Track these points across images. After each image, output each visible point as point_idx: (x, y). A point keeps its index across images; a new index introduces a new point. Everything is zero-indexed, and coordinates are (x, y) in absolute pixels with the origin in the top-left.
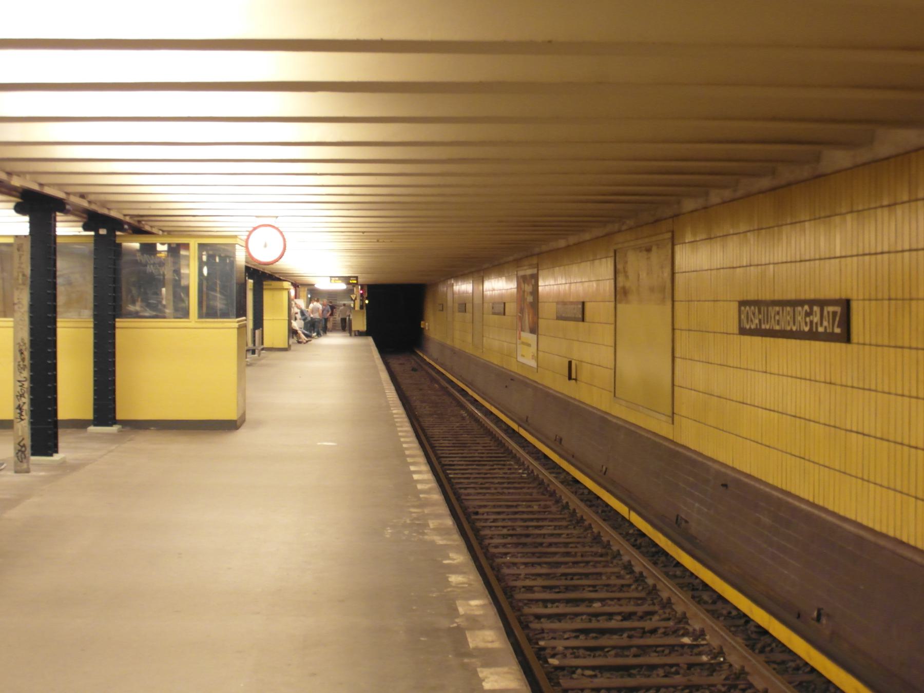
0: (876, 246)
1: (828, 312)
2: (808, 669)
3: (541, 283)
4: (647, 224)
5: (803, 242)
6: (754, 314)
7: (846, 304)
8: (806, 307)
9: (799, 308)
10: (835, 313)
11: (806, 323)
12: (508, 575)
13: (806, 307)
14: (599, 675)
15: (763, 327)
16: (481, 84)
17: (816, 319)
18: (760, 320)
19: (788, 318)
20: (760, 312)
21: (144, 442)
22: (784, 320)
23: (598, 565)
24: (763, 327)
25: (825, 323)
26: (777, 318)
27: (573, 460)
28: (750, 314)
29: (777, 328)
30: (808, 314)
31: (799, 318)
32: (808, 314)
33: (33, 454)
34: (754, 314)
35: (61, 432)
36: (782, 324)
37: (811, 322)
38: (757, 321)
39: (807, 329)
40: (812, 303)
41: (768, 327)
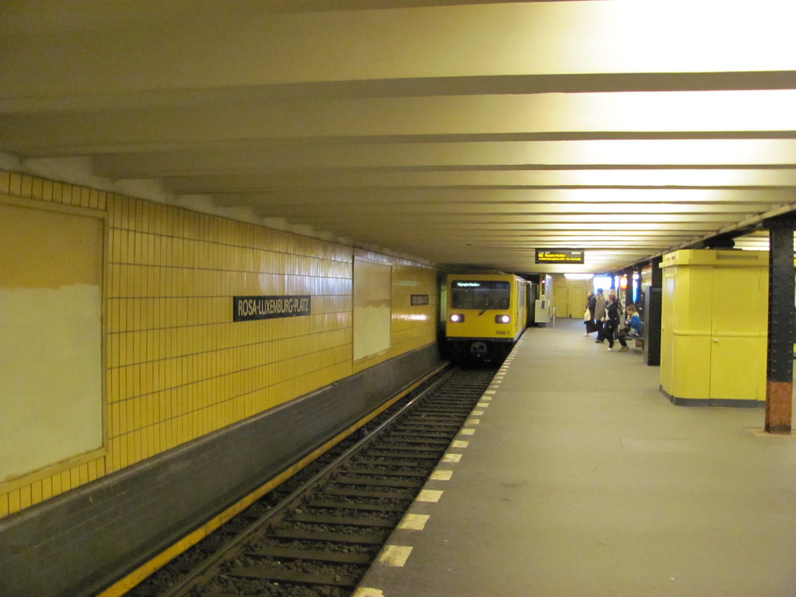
1: (303, 302)
2: (186, 555)
4: (323, 240)
5: (289, 266)
6: (252, 305)
7: (412, 304)
9: (287, 300)
10: (306, 302)
11: (291, 309)
13: (291, 300)
14: (543, 282)
15: (260, 313)
16: (492, 140)
17: (296, 306)
18: (258, 310)
19: (279, 306)
20: (257, 304)
23: (377, 489)
24: (260, 313)
25: (301, 307)
26: (271, 306)
29: (272, 312)
30: (291, 304)
31: (286, 306)
32: (291, 304)
34: (252, 305)
35: (762, 397)
37: (293, 308)
38: (255, 310)
39: (291, 311)
41: (264, 313)
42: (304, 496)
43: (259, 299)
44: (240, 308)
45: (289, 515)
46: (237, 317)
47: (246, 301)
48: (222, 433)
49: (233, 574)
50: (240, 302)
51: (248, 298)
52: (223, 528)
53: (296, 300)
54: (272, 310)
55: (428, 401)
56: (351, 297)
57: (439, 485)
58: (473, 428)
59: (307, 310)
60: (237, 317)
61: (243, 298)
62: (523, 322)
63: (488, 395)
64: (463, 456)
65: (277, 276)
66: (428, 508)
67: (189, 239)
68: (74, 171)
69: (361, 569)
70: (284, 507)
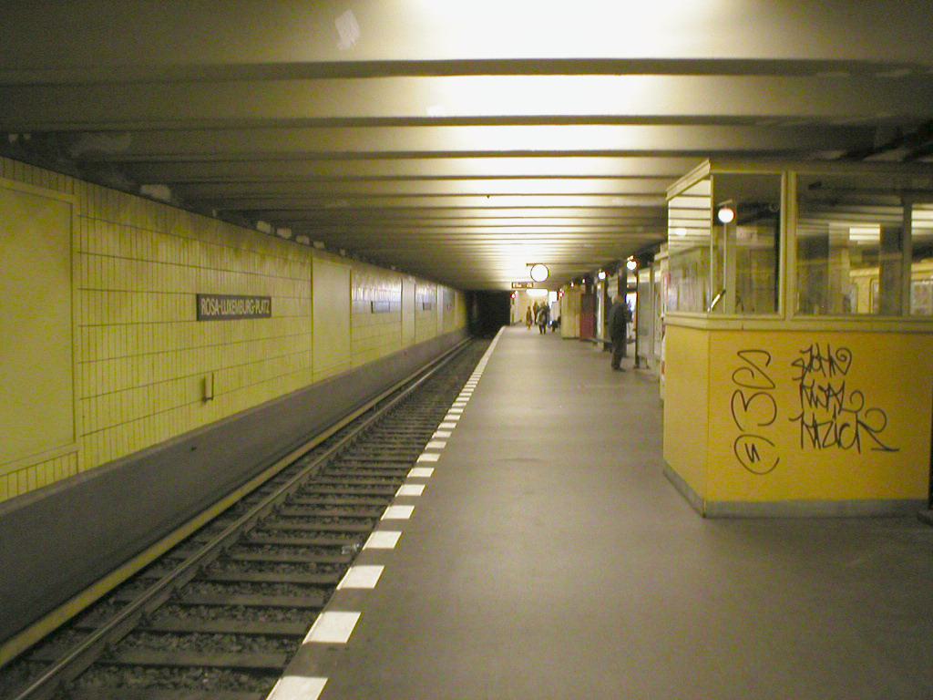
0: (897, 215)
3: (915, 214)
6: (214, 305)
8: (252, 301)
12: (897, 206)
15: (223, 313)
17: (257, 307)
18: (220, 310)
20: (219, 303)
21: (825, 421)
22: (238, 307)
24: (223, 313)
27: (249, 476)
28: (211, 304)
30: (252, 305)
31: (248, 307)
33: (797, 176)
34: (214, 305)
36: (237, 311)
38: (217, 310)
39: (252, 313)
40: (254, 298)
41: (226, 313)
42: (144, 615)
43: (220, 298)
44: (203, 307)
45: (146, 622)
46: (200, 317)
47: (208, 300)
48: (53, 491)
49: (153, 628)
50: (203, 300)
51: (210, 296)
52: (239, 504)
53: (258, 302)
54: (234, 310)
55: (364, 439)
56: (713, 334)
57: (393, 525)
58: (410, 504)
59: (268, 312)
60: (200, 317)
61: (206, 296)
62: (322, 617)
63: (443, 430)
64: (402, 534)
65: (160, 260)
66: (356, 600)
67: (151, 231)
68: (162, 192)
69: (290, 652)
70: (308, 472)
